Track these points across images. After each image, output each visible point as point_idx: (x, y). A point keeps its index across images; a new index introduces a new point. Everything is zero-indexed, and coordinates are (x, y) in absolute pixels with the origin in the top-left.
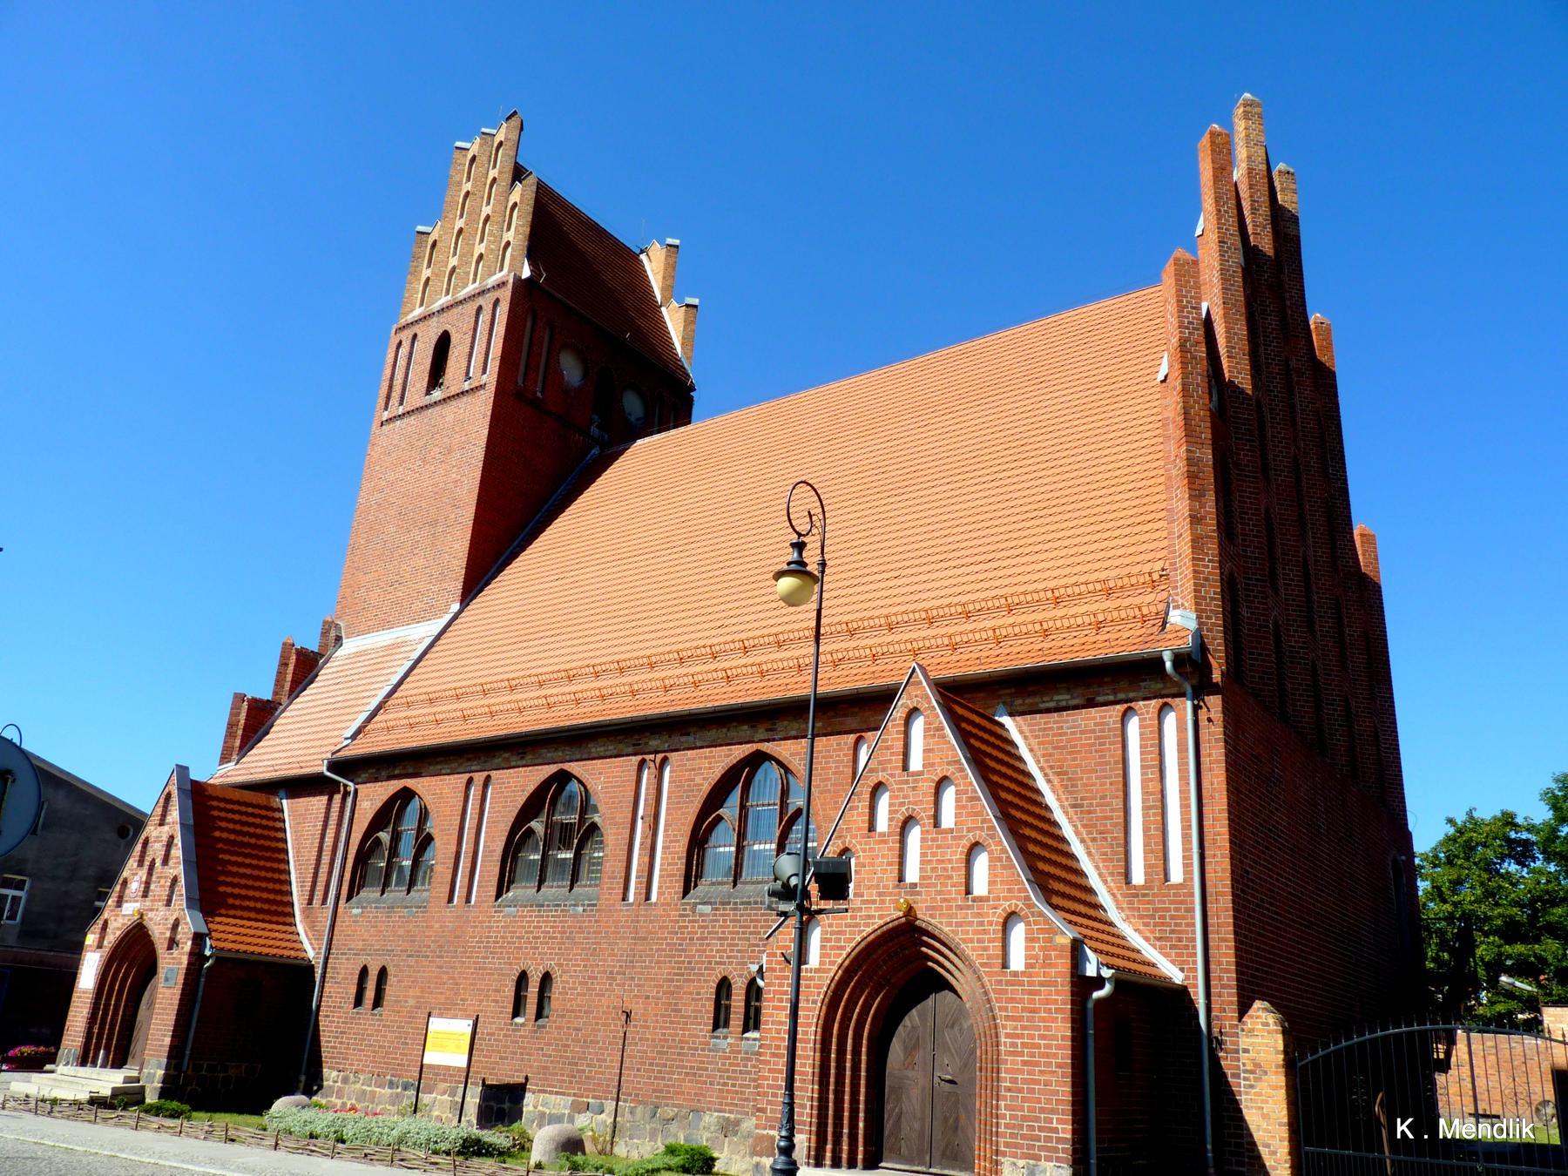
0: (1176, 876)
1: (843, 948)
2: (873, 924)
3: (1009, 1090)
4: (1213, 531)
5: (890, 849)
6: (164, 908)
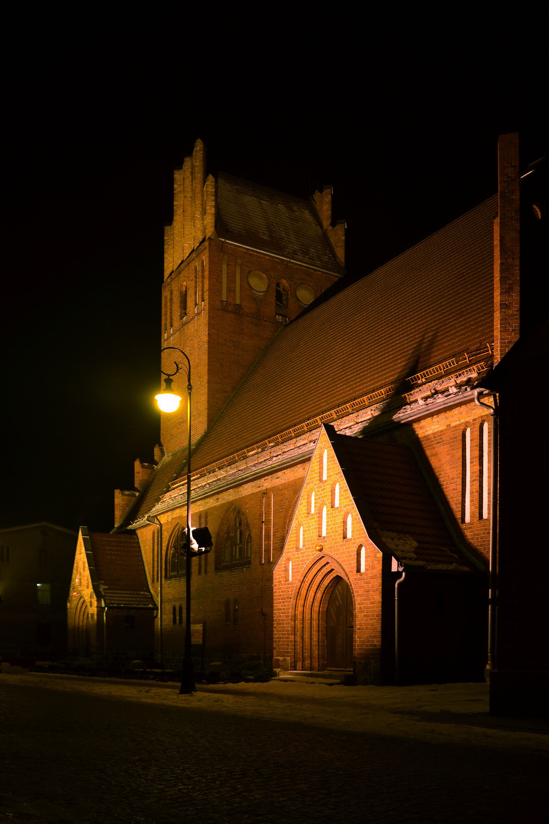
0: (485, 516)
1: (299, 572)
2: (310, 558)
3: (359, 629)
4: (517, 311)
5: (315, 521)
6: (87, 589)
